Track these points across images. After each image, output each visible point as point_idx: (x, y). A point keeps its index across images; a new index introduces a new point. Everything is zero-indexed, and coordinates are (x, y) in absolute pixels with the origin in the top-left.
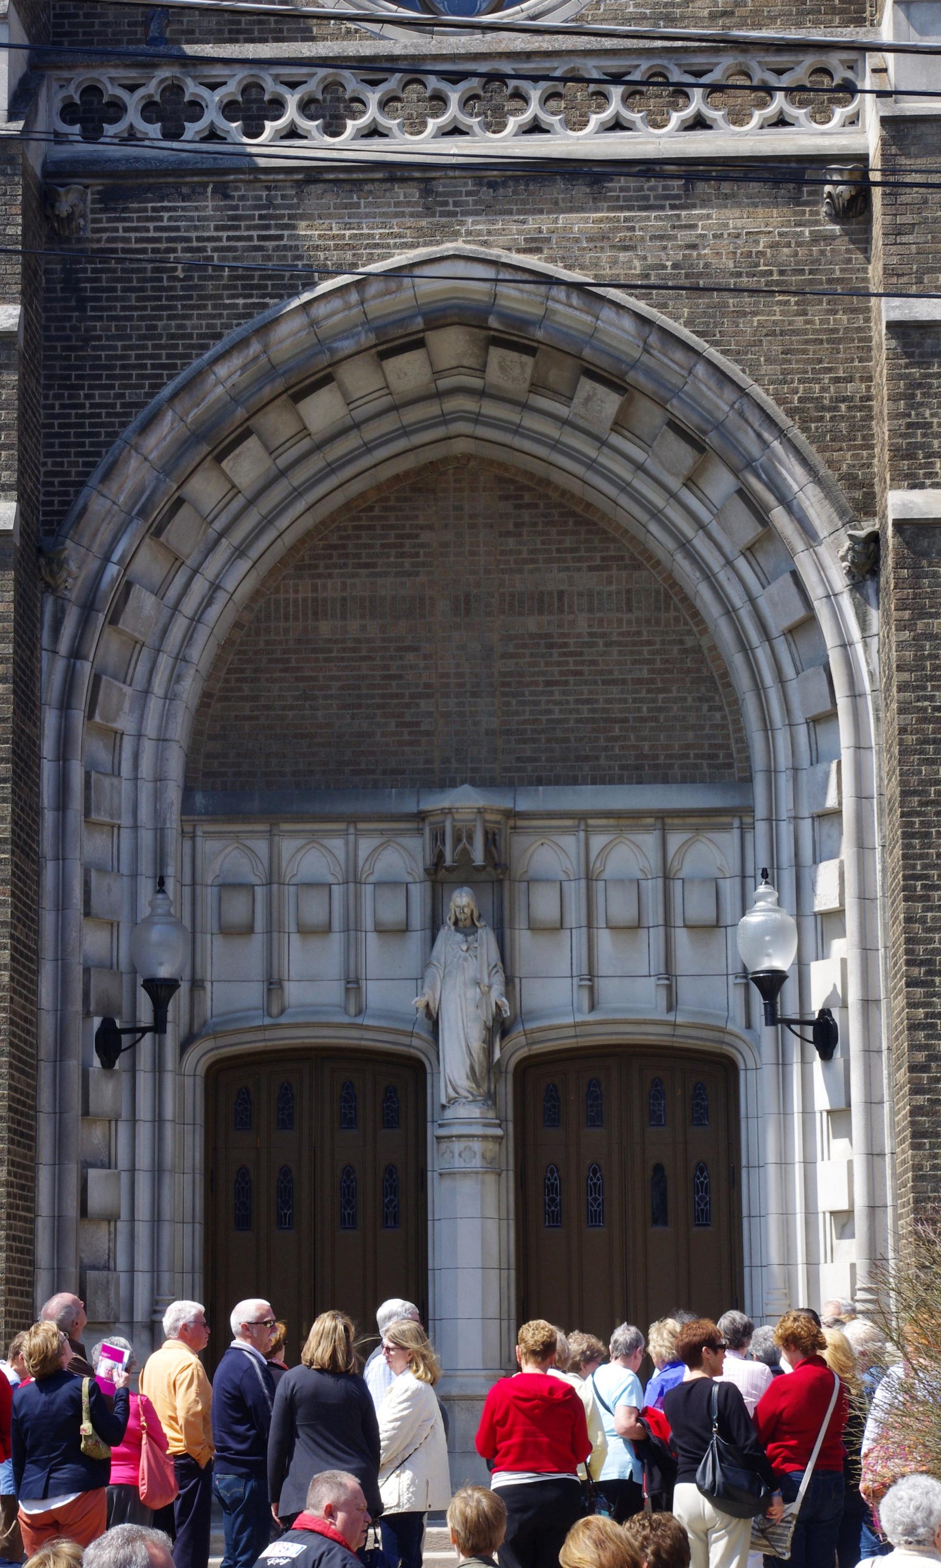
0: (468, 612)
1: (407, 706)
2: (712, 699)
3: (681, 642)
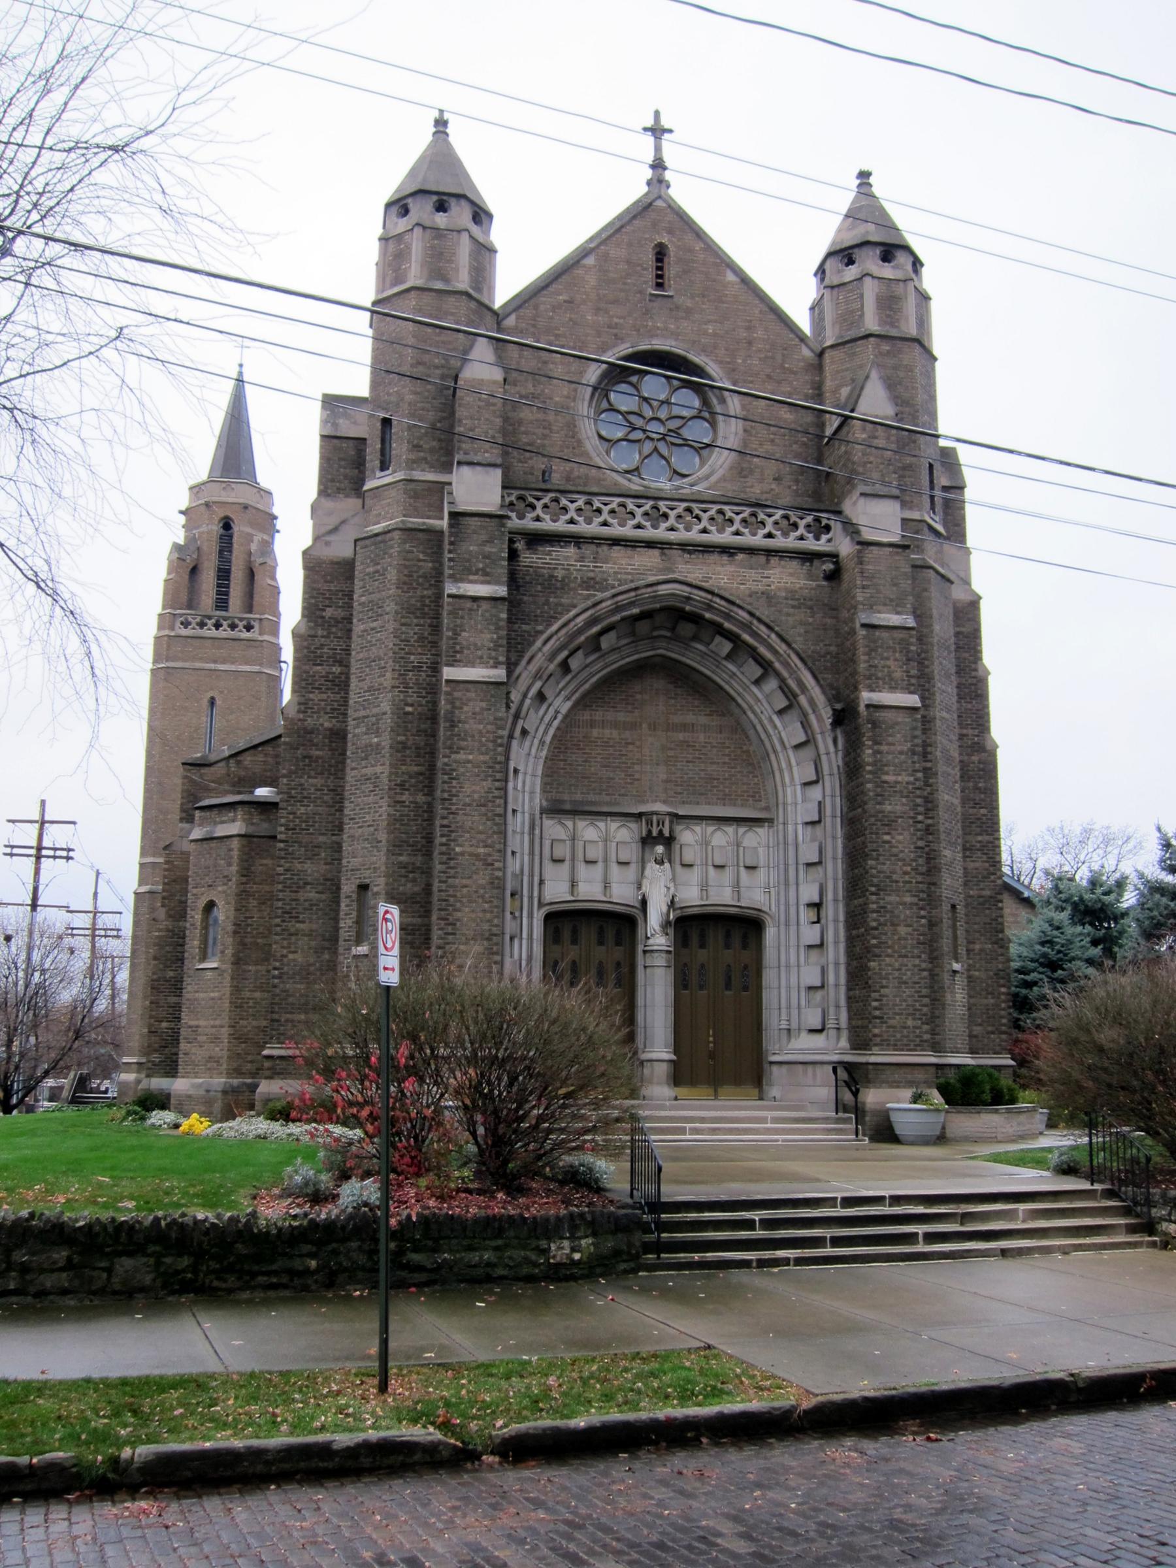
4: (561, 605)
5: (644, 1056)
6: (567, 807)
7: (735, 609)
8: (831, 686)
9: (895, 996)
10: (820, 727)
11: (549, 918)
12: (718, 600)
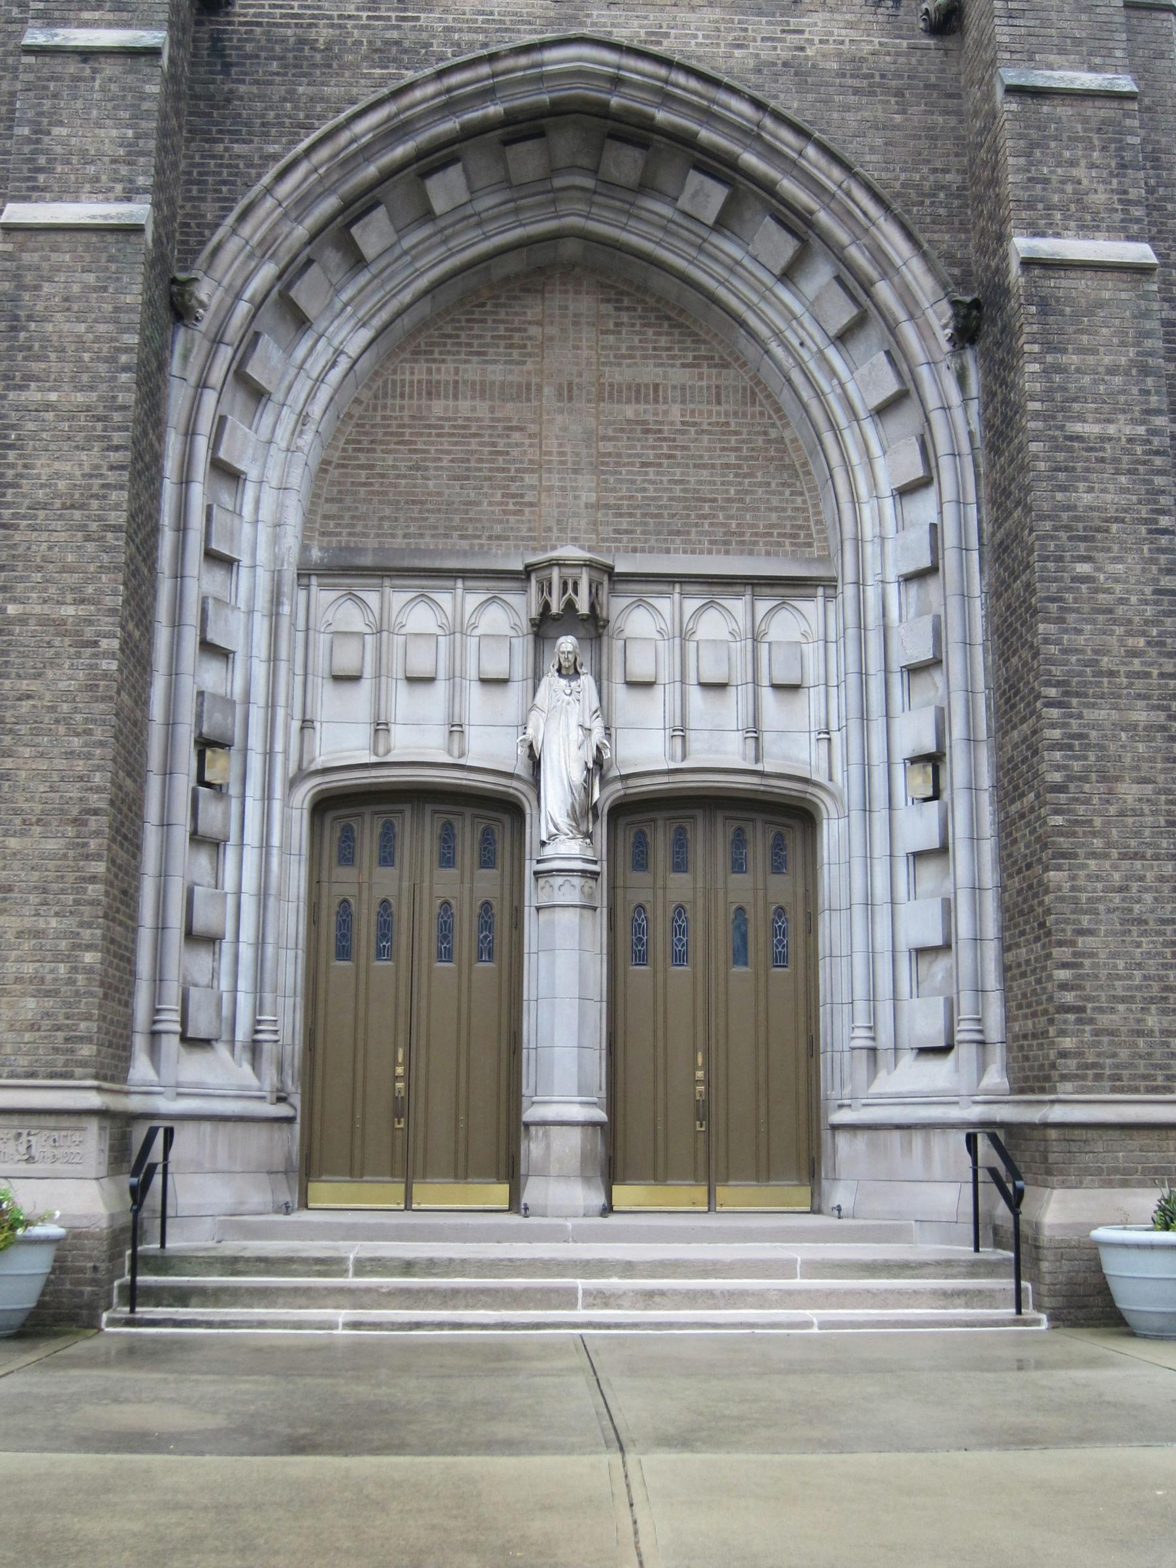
0: (570, 399)
1: (513, 479)
2: (793, 485)
3: (765, 433)
4: (323, 99)
5: (529, 1115)
6: (367, 560)
7: (723, 96)
8: (950, 259)
9: (1114, 955)
10: (928, 350)
11: (325, 806)
12: (681, 79)
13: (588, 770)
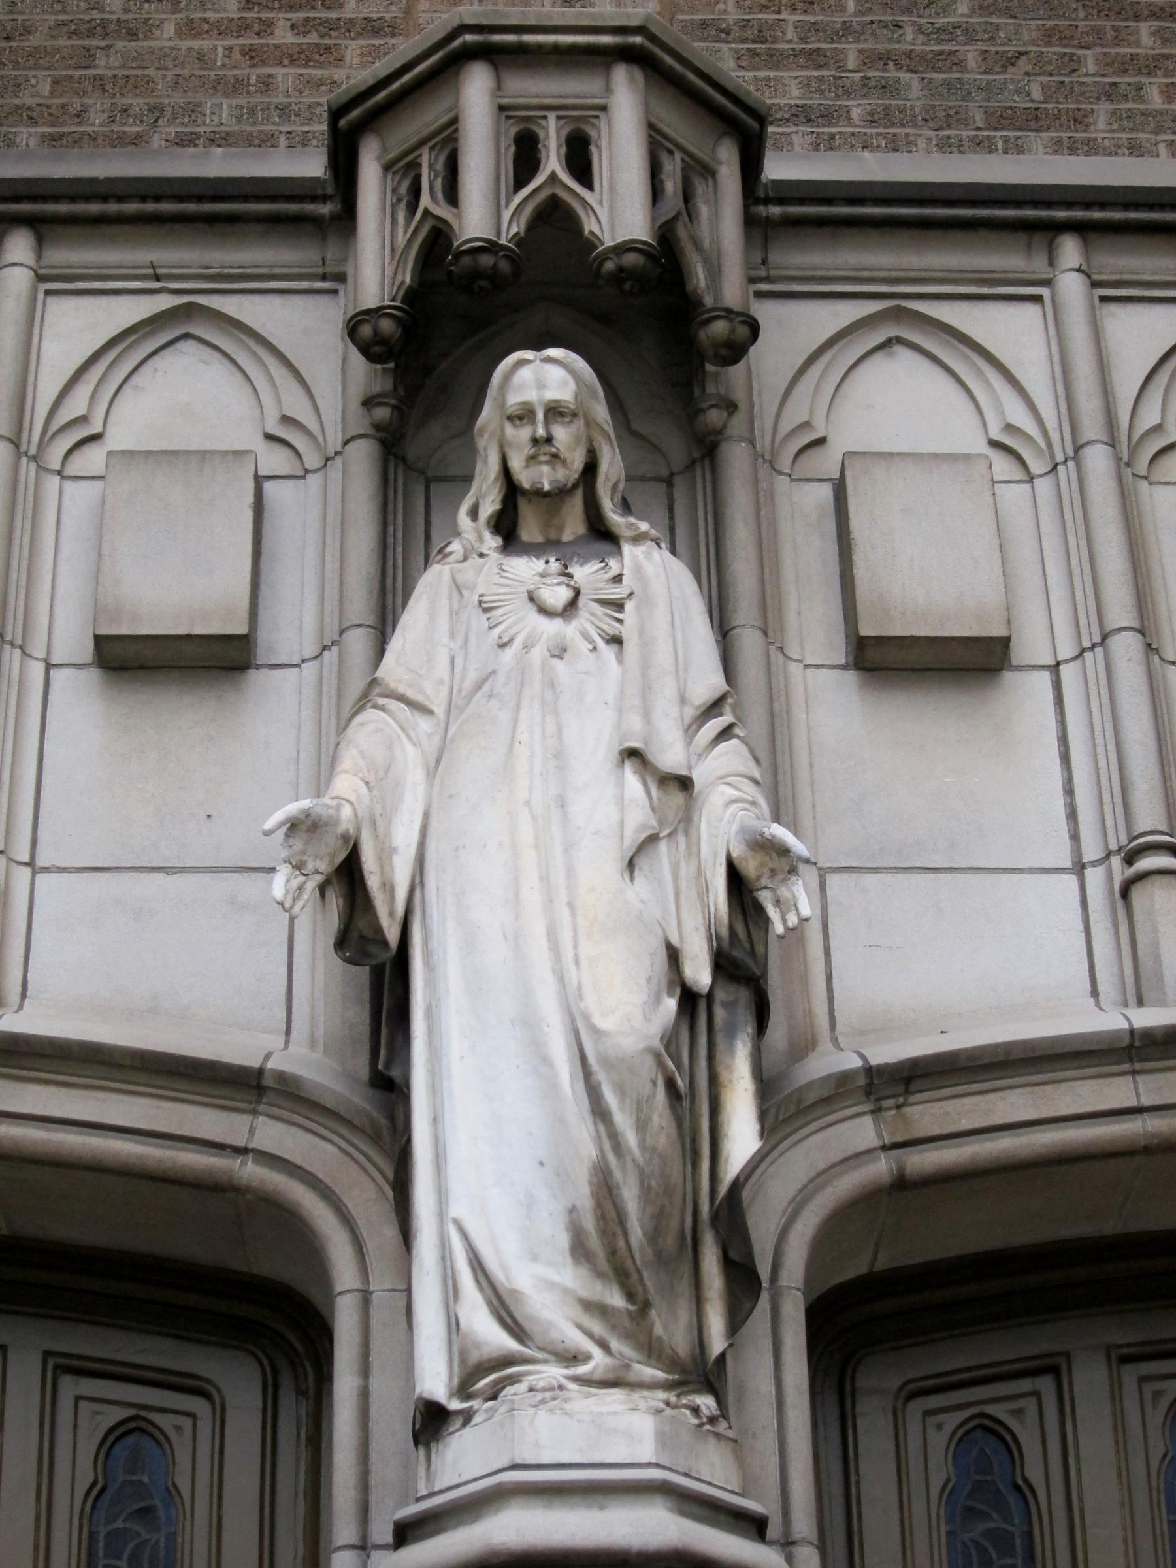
13: (689, 999)
